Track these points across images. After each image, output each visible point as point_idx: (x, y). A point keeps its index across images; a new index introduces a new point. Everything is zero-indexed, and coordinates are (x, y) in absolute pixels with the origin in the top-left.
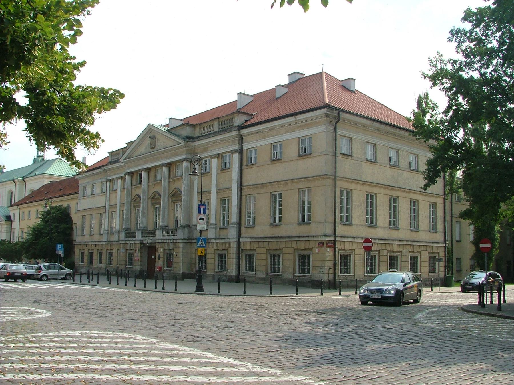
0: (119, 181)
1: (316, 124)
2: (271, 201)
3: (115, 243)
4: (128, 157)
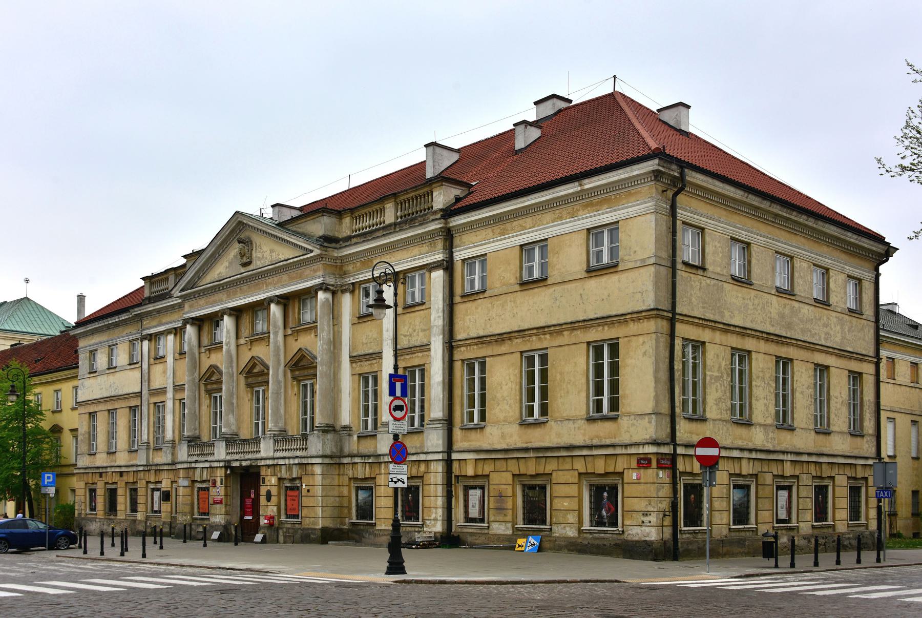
0: (171, 338)
2: (521, 372)
3: (166, 467)
4: (191, 284)
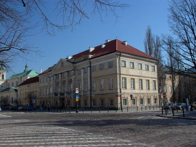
0: (52, 77)
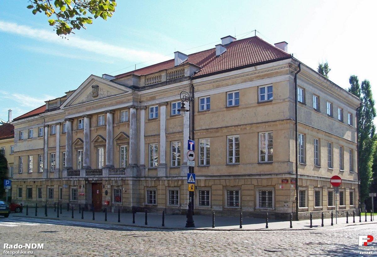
1: (281, 74)
4: (69, 105)
